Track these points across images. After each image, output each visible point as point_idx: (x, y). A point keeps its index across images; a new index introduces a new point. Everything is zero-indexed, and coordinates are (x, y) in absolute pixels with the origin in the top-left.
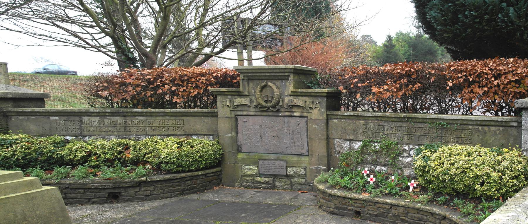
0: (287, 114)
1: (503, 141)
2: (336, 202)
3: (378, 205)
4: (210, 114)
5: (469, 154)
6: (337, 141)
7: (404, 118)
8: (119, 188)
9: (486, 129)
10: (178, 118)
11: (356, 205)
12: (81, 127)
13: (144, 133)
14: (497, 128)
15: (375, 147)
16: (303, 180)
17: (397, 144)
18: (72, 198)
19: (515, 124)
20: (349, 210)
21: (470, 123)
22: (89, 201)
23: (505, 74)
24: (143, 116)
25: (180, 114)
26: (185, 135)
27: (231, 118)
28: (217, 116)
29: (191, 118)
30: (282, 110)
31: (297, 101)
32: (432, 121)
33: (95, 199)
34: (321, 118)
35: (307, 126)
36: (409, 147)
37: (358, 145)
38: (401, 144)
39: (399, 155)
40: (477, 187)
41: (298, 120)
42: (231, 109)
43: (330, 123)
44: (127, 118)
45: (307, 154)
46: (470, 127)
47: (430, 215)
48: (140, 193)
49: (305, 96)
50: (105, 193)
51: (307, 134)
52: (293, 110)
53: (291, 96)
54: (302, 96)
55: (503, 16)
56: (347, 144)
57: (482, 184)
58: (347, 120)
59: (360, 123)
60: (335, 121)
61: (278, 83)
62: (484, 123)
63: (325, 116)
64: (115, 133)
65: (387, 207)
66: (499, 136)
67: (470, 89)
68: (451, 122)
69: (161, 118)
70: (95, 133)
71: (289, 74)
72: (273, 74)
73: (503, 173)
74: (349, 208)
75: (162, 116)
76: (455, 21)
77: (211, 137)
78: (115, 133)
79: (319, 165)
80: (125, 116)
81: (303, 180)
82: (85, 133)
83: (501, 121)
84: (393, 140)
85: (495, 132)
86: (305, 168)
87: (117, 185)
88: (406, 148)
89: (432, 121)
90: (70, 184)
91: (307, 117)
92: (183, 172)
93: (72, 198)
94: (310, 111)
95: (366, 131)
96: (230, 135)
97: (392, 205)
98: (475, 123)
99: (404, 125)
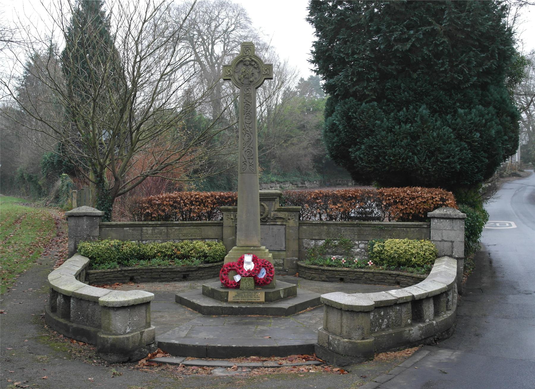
0: (272, 223)
1: (419, 236)
2: (328, 274)
3: (356, 273)
4: (218, 225)
5: (404, 243)
6: (305, 241)
7: (357, 224)
8: (189, 271)
9: (408, 229)
10: (198, 227)
11: (341, 274)
12: (141, 235)
13: (178, 238)
14: (415, 229)
15: (335, 243)
16: (281, 268)
17: (350, 241)
18: (163, 278)
19: (426, 226)
20: (337, 278)
21: (399, 226)
22: (173, 280)
23: (417, 197)
24: (178, 226)
25: (200, 225)
26: (202, 239)
27: (233, 226)
28: (222, 225)
29: (206, 227)
30: (269, 221)
31: (281, 215)
32: (375, 226)
33: (177, 279)
34: (295, 226)
35: (285, 231)
36: (358, 242)
37: (321, 243)
38: (353, 241)
39: (352, 247)
40: (413, 259)
41: (279, 227)
42: (233, 221)
43: (301, 229)
44: (169, 228)
45: (285, 249)
46: (399, 229)
47: (388, 275)
48: (198, 274)
49: (285, 211)
50: (180, 275)
51: (285, 236)
52: (277, 221)
53: (275, 211)
54: (283, 211)
55: (410, 161)
56: (313, 242)
57: (415, 258)
58: (314, 227)
59: (324, 228)
60: (305, 227)
61: (267, 203)
62: (407, 226)
63: (298, 224)
64: (161, 238)
65: (362, 274)
66: (416, 233)
67: (396, 206)
68: (387, 226)
69: (188, 228)
70: (149, 238)
71: (277, 197)
72: (266, 197)
73: (425, 252)
74: (337, 276)
75: (189, 226)
76: (377, 161)
77: (217, 240)
78: (161, 238)
79: (293, 257)
80: (167, 227)
81: (281, 268)
82: (144, 239)
83: (418, 225)
84: (347, 238)
85: (413, 231)
86: (283, 260)
87: (188, 269)
88: (357, 243)
89: (375, 226)
90: (164, 269)
91: (285, 225)
92: (216, 262)
93: (163, 278)
94: (288, 221)
95: (328, 233)
96: (231, 238)
97: (365, 272)
98: (402, 226)
99: (355, 228)
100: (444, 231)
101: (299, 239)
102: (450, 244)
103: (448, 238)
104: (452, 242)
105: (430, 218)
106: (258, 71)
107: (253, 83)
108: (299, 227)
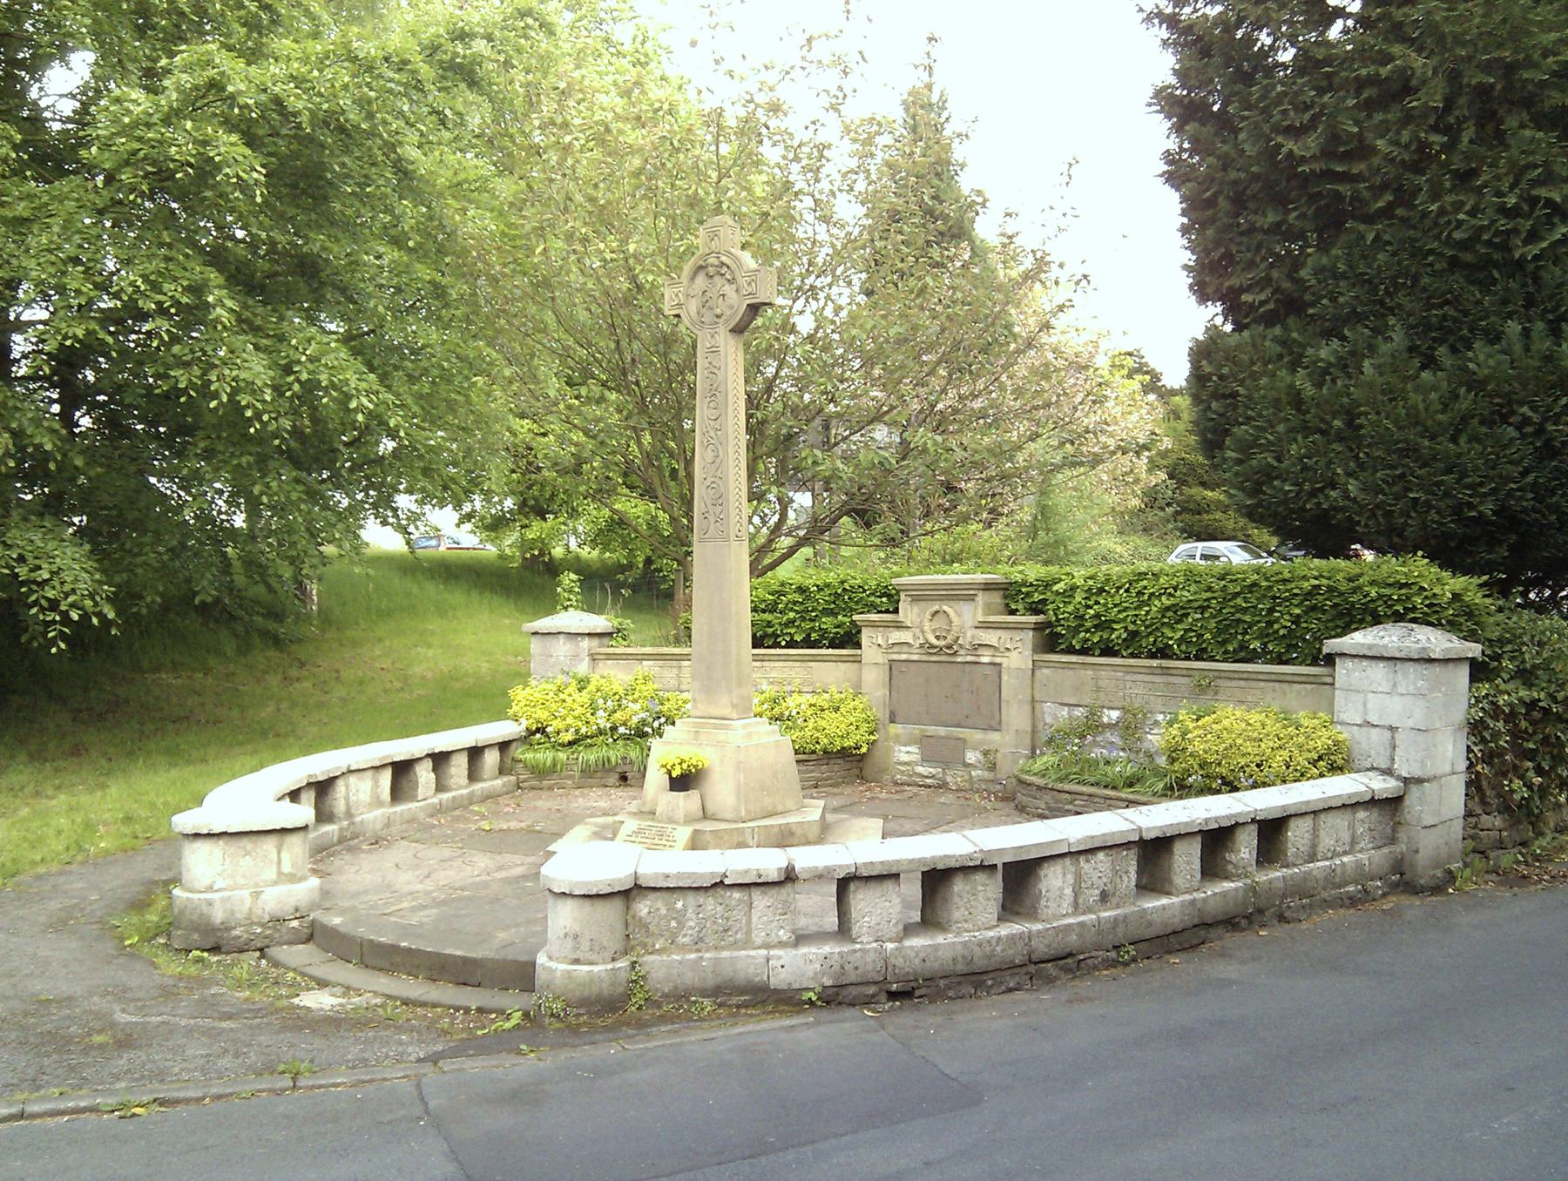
10: (804, 665)
30: (962, 652)
60: (1046, 671)
100: (1371, 695)
101: (1033, 700)
102: (1388, 734)
103: (1380, 718)
104: (1392, 729)
105: (1330, 660)
106: (734, 287)
107: (724, 318)
108: (1033, 670)
